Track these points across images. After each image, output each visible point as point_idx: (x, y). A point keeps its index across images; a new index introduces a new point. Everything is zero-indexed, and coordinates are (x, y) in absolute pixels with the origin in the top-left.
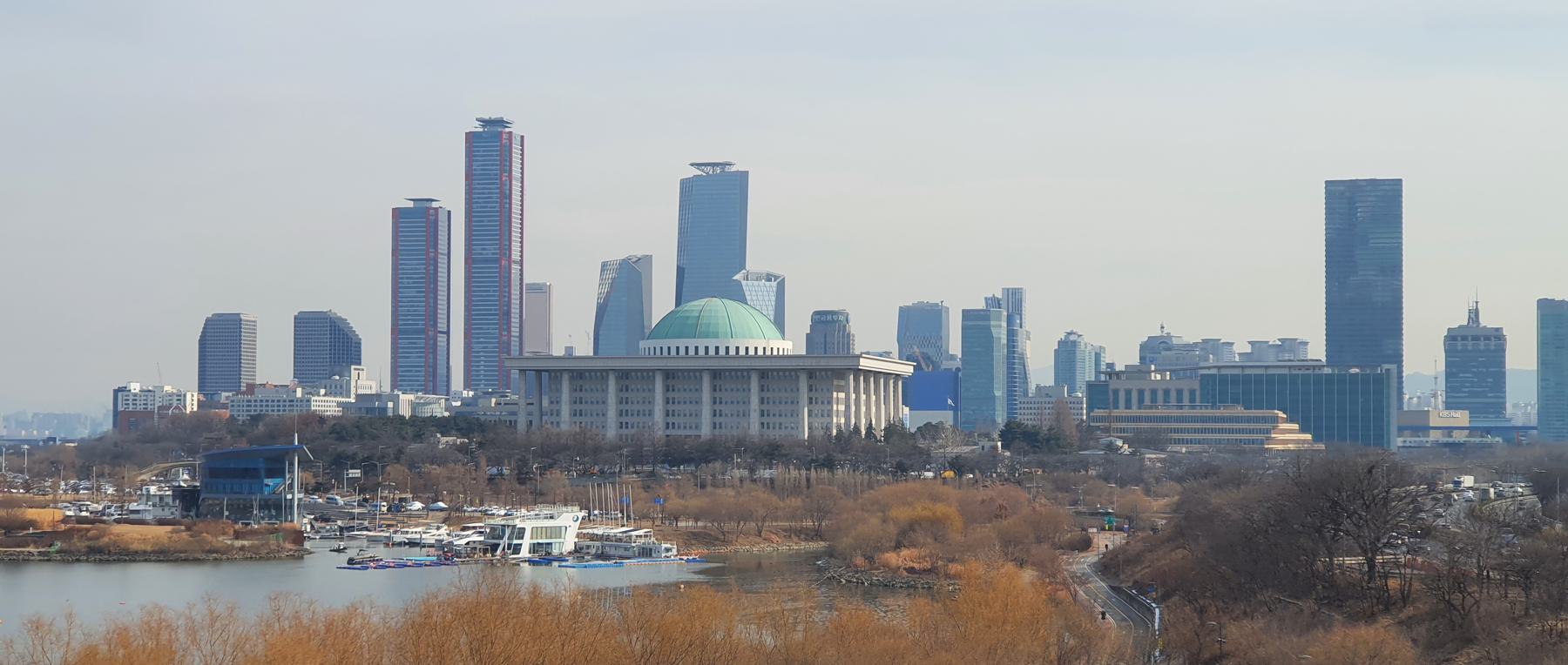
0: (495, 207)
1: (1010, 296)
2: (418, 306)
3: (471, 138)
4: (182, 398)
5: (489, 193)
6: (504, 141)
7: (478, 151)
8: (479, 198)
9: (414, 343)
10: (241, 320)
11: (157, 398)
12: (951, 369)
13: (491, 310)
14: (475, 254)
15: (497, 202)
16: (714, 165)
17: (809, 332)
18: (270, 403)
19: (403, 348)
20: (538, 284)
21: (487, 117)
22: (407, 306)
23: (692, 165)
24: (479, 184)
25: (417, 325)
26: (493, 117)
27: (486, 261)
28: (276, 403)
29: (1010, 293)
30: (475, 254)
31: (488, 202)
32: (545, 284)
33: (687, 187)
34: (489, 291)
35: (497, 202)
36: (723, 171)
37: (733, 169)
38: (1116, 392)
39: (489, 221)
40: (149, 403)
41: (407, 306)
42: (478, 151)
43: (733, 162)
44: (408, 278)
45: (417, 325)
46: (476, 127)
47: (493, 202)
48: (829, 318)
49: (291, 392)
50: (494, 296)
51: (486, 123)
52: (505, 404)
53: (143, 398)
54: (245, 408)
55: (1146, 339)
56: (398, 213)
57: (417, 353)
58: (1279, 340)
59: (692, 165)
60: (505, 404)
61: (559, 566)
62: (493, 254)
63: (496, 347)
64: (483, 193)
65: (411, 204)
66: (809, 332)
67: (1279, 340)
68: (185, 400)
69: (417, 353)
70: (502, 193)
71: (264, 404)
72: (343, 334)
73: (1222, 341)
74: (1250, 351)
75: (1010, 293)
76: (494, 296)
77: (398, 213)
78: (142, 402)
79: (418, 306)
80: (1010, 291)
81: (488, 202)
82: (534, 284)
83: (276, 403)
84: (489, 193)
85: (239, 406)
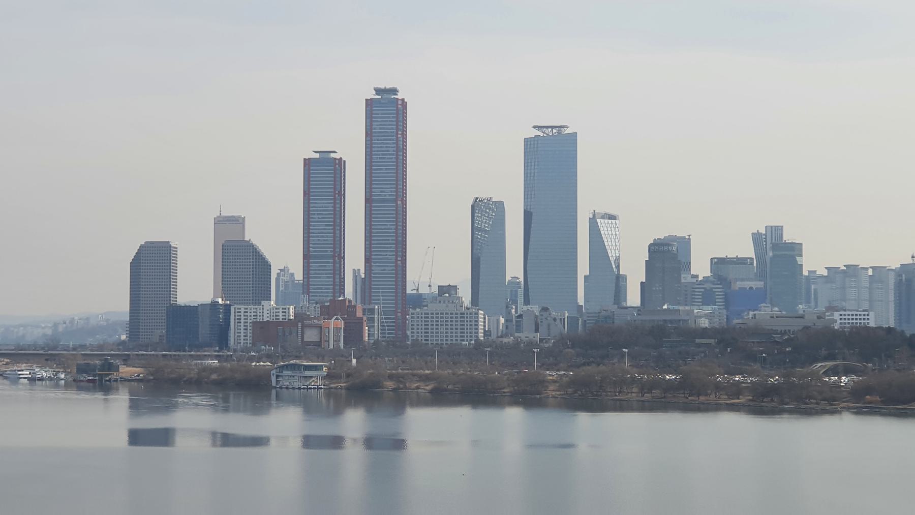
0: (392, 159)
1: (773, 232)
2: (327, 237)
3: (369, 103)
4: (287, 311)
5: (387, 147)
6: (399, 106)
7: (378, 114)
8: (378, 151)
9: (325, 266)
10: (170, 246)
11: (265, 311)
12: (746, 288)
13: (388, 240)
14: (375, 195)
15: (393, 154)
16: (552, 127)
17: (648, 259)
18: (444, 316)
19: (315, 270)
20: (234, 217)
21: (383, 87)
22: (318, 237)
23: (534, 127)
24: (378, 140)
25: (327, 251)
26: (388, 87)
27: (384, 201)
28: (449, 316)
29: (773, 230)
30: (375, 195)
31: (386, 154)
32: (240, 217)
33: (529, 143)
34: (386, 225)
35: (393, 154)
36: (559, 132)
37: (568, 131)
38: (283, 319)
39: (386, 169)
40: (258, 314)
41: (318, 237)
42: (378, 114)
43: (569, 126)
44: (318, 214)
45: (327, 251)
46: (372, 95)
47: (390, 154)
48: (666, 248)
49: (458, 307)
50: (391, 229)
51: (378, 91)
52: (777, 317)
53: (253, 310)
54: (423, 319)
55: (899, 266)
56: (308, 162)
57: (326, 274)
58: (845, 266)
59: (534, 127)
60: (777, 317)
61: (227, 440)
62: (390, 195)
63: (392, 270)
64: (381, 147)
65: (317, 156)
66: (648, 259)
67: (845, 266)
68: (289, 313)
69: (326, 274)
70: (397, 147)
71: (439, 316)
72: (259, 256)
73: (860, 266)
74: (826, 274)
75: (773, 230)
76: (391, 229)
77: (308, 162)
78: (253, 314)
79: (327, 237)
80: (773, 228)
81: (386, 154)
82: (232, 216)
83: (449, 316)
84: (387, 147)
85: (418, 317)
